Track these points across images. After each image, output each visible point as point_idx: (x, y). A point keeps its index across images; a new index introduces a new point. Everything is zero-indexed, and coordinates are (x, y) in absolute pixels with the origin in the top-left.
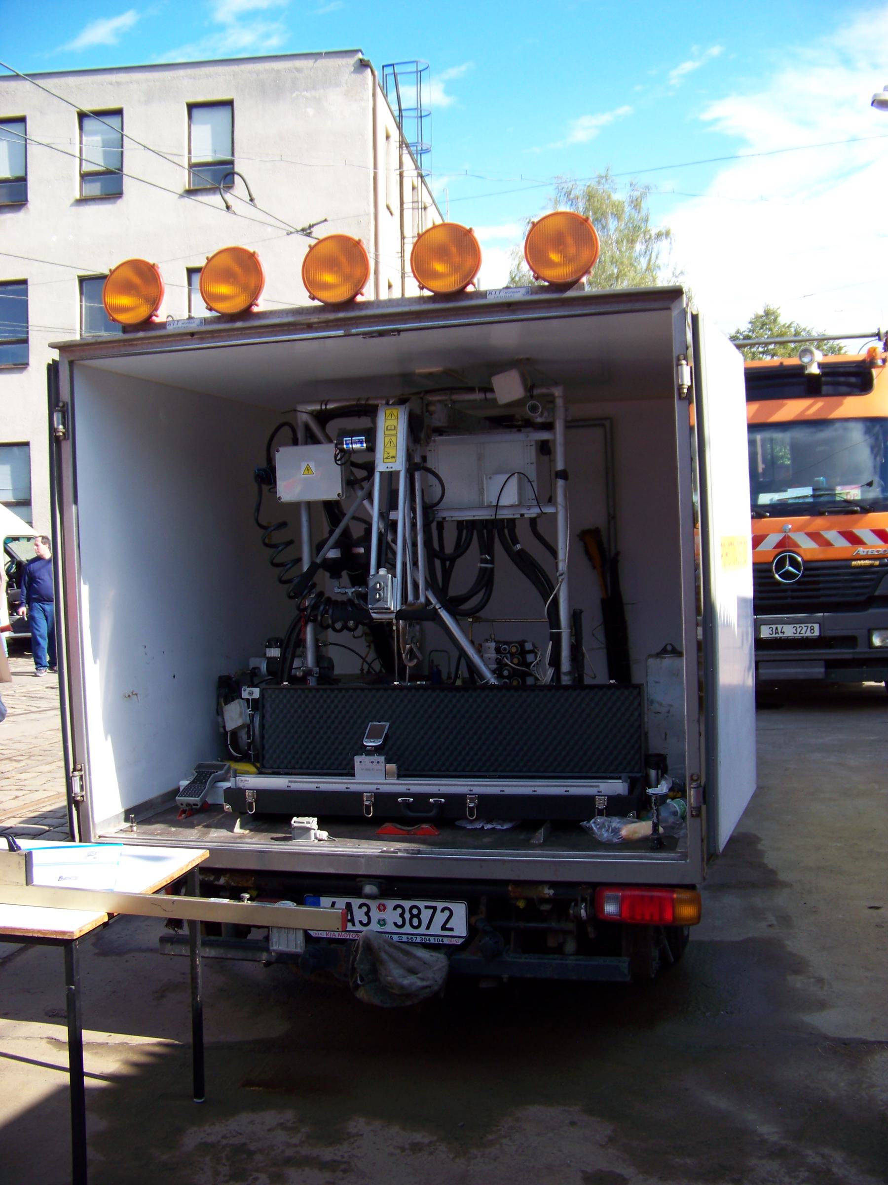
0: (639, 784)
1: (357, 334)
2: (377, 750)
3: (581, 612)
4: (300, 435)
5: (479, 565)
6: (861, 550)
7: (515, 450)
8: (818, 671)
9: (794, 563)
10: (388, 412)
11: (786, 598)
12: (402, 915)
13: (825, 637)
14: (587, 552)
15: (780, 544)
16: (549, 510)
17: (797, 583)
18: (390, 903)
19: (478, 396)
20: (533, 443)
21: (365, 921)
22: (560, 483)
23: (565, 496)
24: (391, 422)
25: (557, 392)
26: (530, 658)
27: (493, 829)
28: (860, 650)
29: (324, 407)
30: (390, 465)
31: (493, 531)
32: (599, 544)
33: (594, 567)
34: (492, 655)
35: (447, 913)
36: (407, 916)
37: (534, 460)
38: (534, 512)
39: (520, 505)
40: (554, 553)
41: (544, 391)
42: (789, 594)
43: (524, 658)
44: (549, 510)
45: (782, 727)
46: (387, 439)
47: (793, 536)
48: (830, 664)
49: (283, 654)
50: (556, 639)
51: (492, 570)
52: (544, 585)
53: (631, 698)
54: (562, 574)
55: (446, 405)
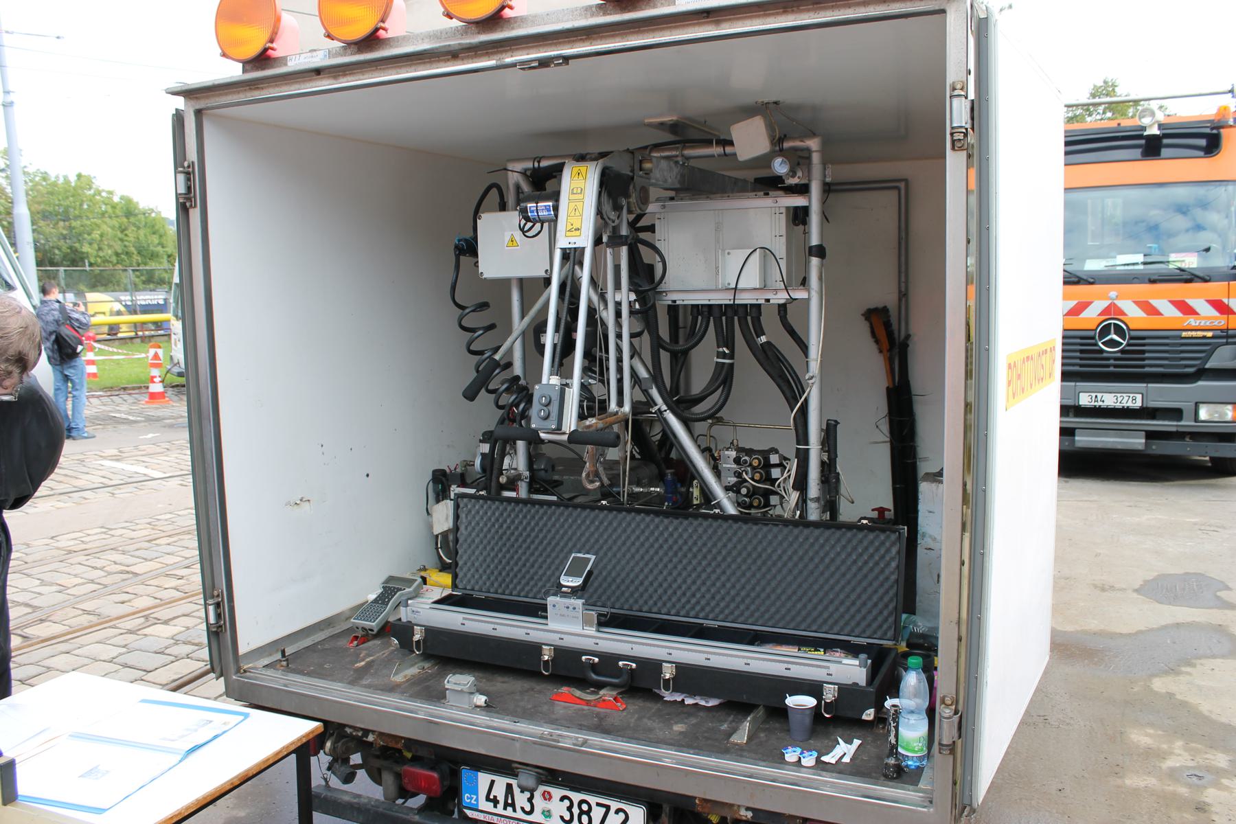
0: (885, 681)
1: (513, 65)
2: (575, 592)
3: (837, 423)
4: (511, 199)
5: (716, 360)
6: (1192, 321)
7: (764, 218)
8: (1137, 442)
9: (1119, 331)
10: (576, 170)
11: (1108, 366)
12: (570, 809)
13: (1147, 408)
14: (873, 334)
15: (1106, 311)
16: (800, 294)
17: (1122, 351)
18: (557, 793)
19: (716, 150)
20: (783, 210)
21: (528, 808)
22: (815, 261)
23: (820, 279)
24: (578, 183)
25: (813, 144)
26: (775, 473)
27: (696, 704)
28: (1186, 423)
29: (536, 165)
30: (572, 240)
31: (735, 319)
32: (887, 325)
33: (881, 352)
34: (728, 465)
35: (622, 816)
36: (576, 811)
37: (783, 232)
38: (781, 297)
39: (764, 288)
40: (804, 348)
41: (798, 144)
42: (1112, 362)
43: (769, 474)
44: (800, 294)
45: (1095, 498)
46: (572, 205)
47: (1120, 303)
48: (1151, 435)
49: (492, 449)
50: (803, 457)
51: (732, 365)
52: (792, 388)
53: (888, 544)
54: (811, 378)
55: (677, 162)
